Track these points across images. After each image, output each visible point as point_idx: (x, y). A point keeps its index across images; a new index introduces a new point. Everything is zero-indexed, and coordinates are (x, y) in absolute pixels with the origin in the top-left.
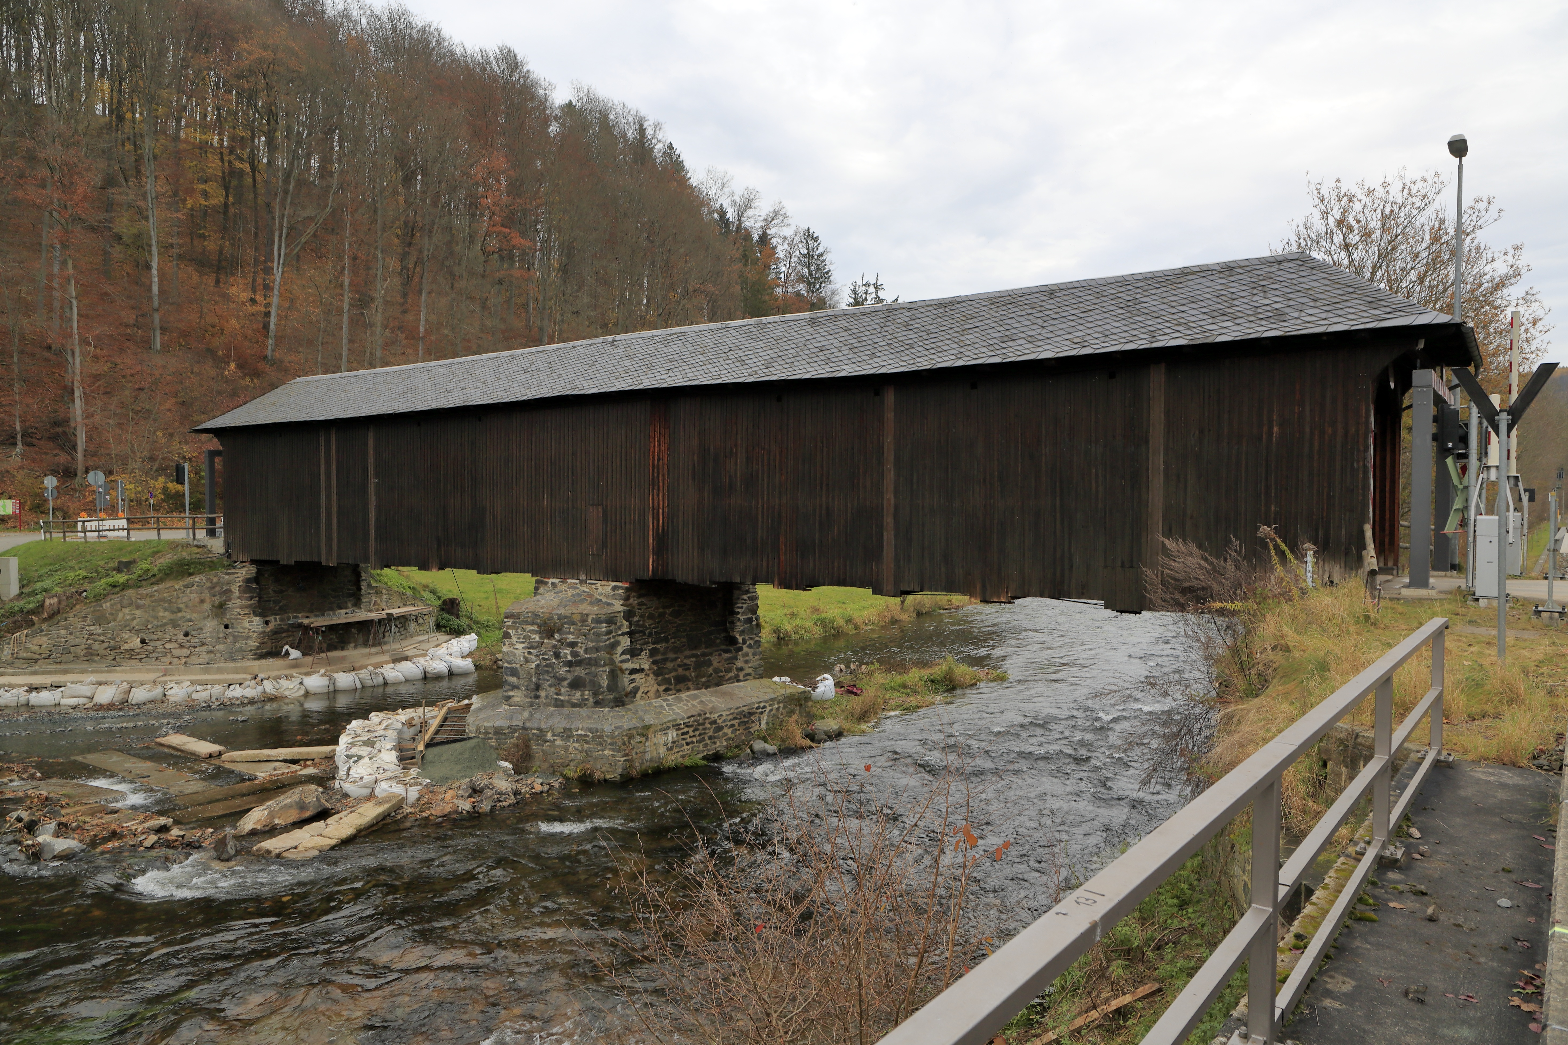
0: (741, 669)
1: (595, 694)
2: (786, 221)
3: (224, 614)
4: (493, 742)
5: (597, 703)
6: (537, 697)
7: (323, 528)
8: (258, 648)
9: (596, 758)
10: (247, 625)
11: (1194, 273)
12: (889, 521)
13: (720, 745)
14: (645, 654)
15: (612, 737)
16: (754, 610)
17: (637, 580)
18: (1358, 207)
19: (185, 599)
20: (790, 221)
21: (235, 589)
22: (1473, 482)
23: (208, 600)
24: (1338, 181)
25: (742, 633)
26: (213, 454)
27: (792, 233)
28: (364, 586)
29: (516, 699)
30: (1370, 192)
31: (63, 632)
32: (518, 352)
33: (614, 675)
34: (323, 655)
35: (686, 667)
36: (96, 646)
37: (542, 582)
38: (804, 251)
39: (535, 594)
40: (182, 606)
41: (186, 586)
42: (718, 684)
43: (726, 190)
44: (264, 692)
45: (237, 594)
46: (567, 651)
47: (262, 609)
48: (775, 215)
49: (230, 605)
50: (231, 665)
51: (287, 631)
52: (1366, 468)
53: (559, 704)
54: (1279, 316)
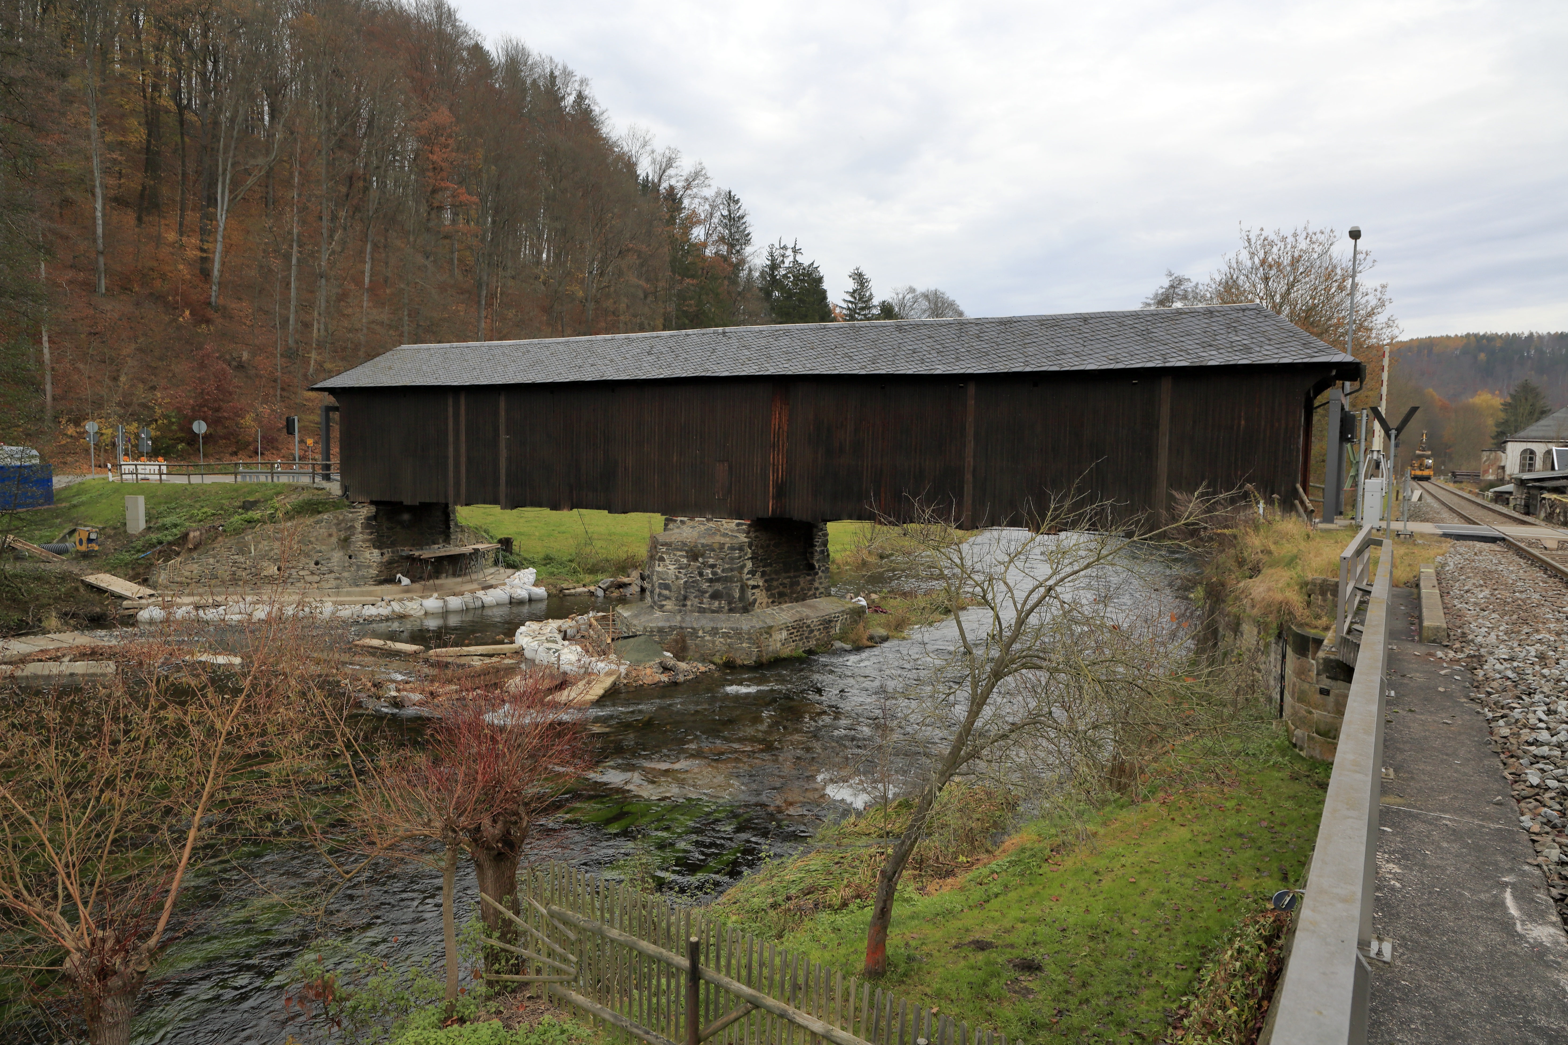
0: (817, 589)
1: (730, 603)
2: (707, 182)
3: (349, 546)
4: (657, 638)
5: (731, 610)
6: (684, 605)
7: (451, 474)
8: (377, 576)
9: (737, 650)
10: (368, 556)
11: (1186, 313)
12: (969, 477)
13: (812, 643)
14: (758, 574)
15: (749, 633)
16: (825, 544)
17: (758, 519)
18: (1275, 249)
19: (315, 534)
20: (711, 182)
21: (358, 526)
22: (1362, 459)
23: (335, 534)
24: (1262, 229)
25: (818, 561)
26: (329, 409)
27: (713, 194)
28: (452, 524)
29: (668, 607)
30: (1284, 239)
31: (211, 561)
32: (632, 335)
33: (743, 588)
34: (431, 582)
35: (784, 585)
36: (239, 573)
37: (672, 520)
38: (725, 213)
39: (665, 530)
40: (312, 539)
41: (317, 523)
42: (804, 600)
43: (648, 148)
44: (393, 611)
45: (360, 529)
46: (709, 571)
47: (379, 544)
48: (697, 175)
49: (353, 539)
50: (357, 589)
51: (397, 562)
52: (1298, 448)
53: (702, 611)
54: (1247, 349)
